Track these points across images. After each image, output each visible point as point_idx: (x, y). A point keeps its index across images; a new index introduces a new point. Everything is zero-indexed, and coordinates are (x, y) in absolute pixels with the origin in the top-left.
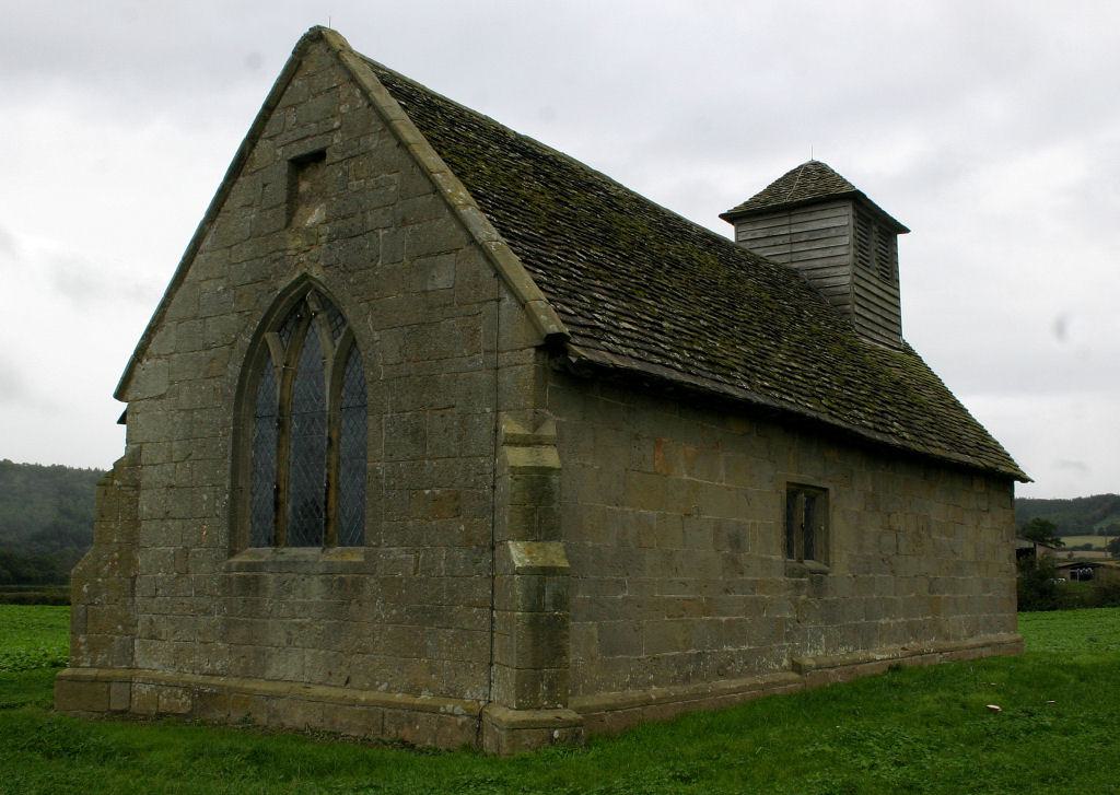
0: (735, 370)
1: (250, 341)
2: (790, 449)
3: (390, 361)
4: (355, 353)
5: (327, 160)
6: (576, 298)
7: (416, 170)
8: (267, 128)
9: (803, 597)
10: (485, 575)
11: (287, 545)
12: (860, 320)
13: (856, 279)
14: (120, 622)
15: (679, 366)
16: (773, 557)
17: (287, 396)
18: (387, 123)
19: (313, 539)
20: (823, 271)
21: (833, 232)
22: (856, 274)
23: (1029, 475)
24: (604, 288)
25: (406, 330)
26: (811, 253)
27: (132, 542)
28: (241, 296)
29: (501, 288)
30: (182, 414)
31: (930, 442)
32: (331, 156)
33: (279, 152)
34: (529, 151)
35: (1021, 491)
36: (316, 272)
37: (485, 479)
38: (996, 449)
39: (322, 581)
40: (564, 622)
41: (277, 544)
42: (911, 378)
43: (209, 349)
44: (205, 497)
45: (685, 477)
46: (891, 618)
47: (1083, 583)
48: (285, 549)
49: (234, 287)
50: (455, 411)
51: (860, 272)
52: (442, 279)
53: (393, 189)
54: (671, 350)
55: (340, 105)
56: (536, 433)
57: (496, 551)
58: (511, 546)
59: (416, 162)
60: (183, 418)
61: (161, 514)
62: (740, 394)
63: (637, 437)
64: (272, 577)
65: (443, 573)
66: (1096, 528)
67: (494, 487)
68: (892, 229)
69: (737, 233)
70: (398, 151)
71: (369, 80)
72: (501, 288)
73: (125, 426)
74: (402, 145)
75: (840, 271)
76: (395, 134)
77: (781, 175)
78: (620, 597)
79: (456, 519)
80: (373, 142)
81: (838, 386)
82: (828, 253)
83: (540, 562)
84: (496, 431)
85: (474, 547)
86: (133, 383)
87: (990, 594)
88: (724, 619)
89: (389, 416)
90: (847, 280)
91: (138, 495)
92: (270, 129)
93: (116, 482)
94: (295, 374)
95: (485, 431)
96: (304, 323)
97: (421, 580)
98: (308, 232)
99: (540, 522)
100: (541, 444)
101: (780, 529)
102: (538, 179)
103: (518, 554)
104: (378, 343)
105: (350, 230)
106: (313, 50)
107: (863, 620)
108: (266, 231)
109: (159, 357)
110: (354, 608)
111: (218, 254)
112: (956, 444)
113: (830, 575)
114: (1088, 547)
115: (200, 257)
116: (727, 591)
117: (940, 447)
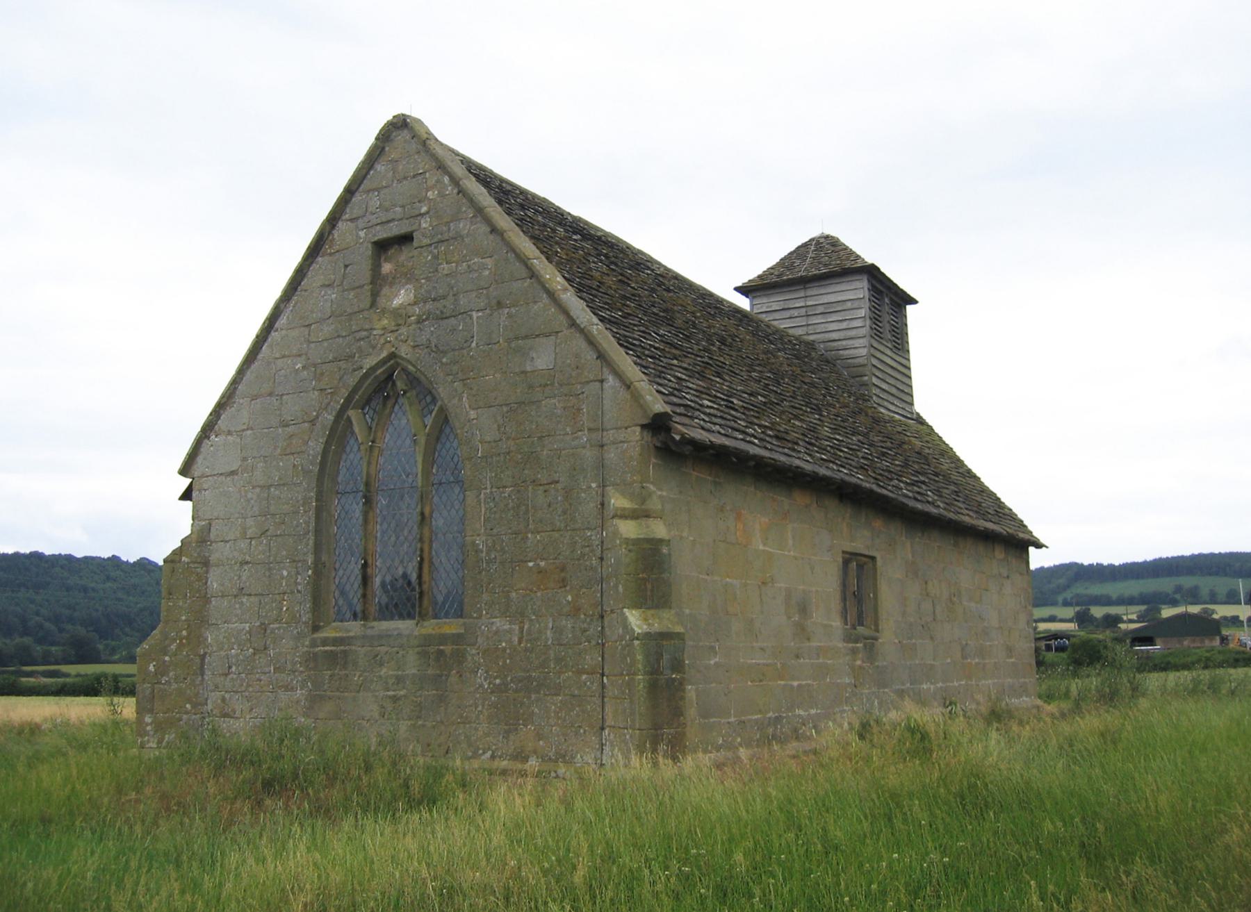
0: (797, 444)
1: (333, 418)
2: (844, 518)
3: (488, 438)
4: (447, 430)
5: (415, 243)
6: (665, 378)
7: (511, 256)
8: (348, 210)
9: (859, 662)
10: (594, 642)
11: (375, 620)
12: (877, 391)
13: (872, 351)
14: (189, 701)
15: (756, 441)
16: (833, 624)
17: (373, 472)
18: (479, 211)
19: (405, 613)
20: (840, 343)
21: (849, 305)
22: (872, 346)
23: (1043, 541)
24: (680, 367)
25: (505, 409)
26: (827, 325)
27: (200, 620)
28: (322, 374)
29: (605, 369)
30: (258, 490)
31: (959, 511)
32: (419, 239)
33: (362, 234)
34: (585, 231)
35: (1037, 559)
36: (404, 351)
37: (592, 551)
38: (1011, 516)
39: (418, 653)
40: (681, 684)
41: (365, 617)
42: (929, 448)
43: (287, 426)
44: (285, 573)
45: (761, 547)
46: (932, 683)
47: (1058, 654)
48: (375, 624)
49: (315, 365)
50: (559, 486)
51: (876, 345)
52: (542, 359)
53: (487, 273)
54: (746, 427)
55: (427, 191)
56: (643, 507)
57: (606, 620)
58: (627, 614)
59: (512, 249)
60: (258, 496)
61: (235, 591)
62: (808, 467)
63: (722, 509)
64: (362, 651)
65: (549, 643)
66: (1060, 599)
67: (602, 559)
68: (902, 300)
69: (752, 306)
70: (491, 237)
71: (459, 171)
72: (605, 369)
73: (188, 505)
74: (494, 230)
75: (857, 343)
76: (488, 220)
77: (793, 248)
78: (712, 662)
79: (563, 589)
80: (463, 226)
81: (878, 458)
82: (844, 325)
83: (657, 627)
84: (602, 504)
85: (582, 616)
86: (200, 459)
87: (1013, 660)
88: (795, 683)
89: (488, 491)
90: (864, 352)
91: (207, 572)
92: (350, 212)
93: (183, 559)
94: (381, 451)
95: (592, 505)
96: (392, 401)
97: (526, 650)
98: (396, 313)
99: (652, 591)
100: (648, 516)
101: (838, 596)
102: (601, 261)
103: (635, 620)
104: (475, 421)
105: (442, 312)
106: (395, 137)
107: (908, 685)
108: (349, 310)
109: (229, 433)
110: (453, 678)
111: (295, 333)
112: (982, 514)
113: (880, 641)
114: (1052, 619)
115: (274, 335)
116: (797, 657)
117: (968, 515)
